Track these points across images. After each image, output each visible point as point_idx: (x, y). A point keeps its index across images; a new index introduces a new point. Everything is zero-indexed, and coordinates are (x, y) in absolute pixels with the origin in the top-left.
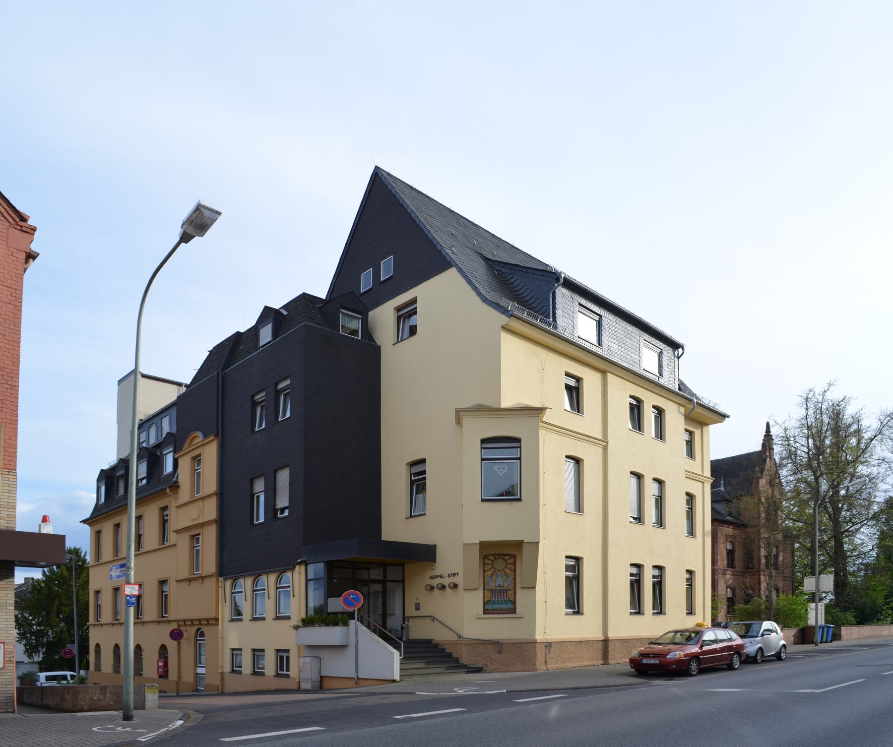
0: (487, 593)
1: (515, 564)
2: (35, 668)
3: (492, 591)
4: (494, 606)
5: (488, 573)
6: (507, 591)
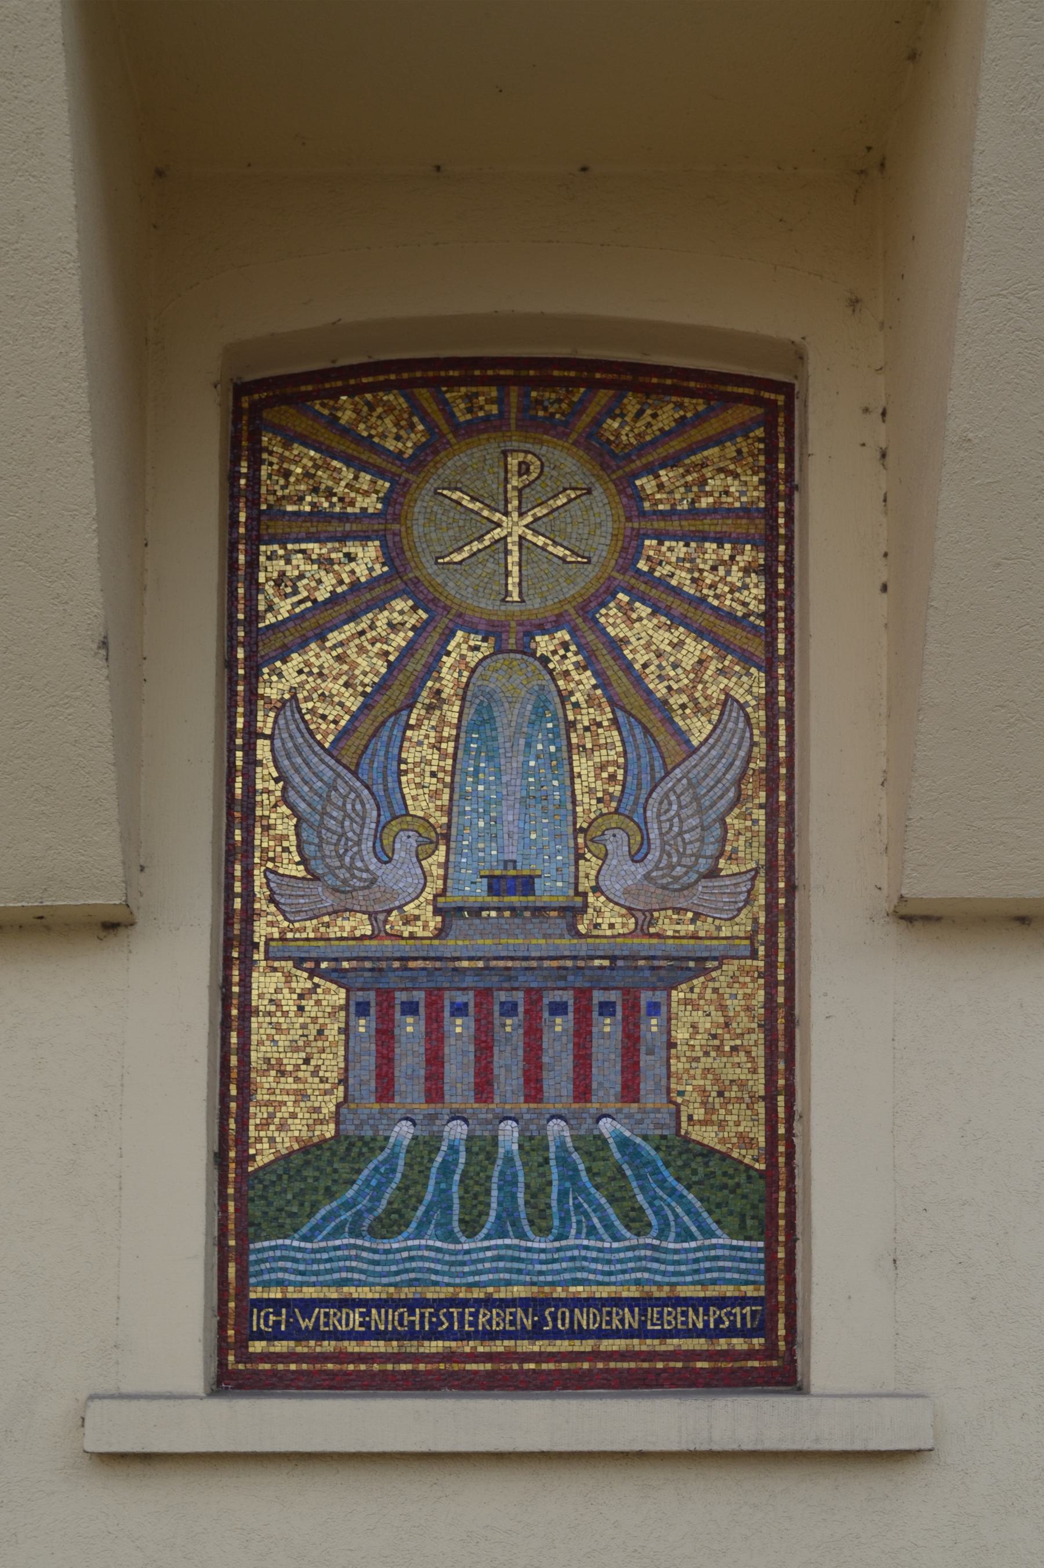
0: (299, 1020)
1: (772, 533)
2: (590, 763)
3: (380, 988)
4: (431, 1260)
5: (323, 681)
6: (637, 983)
